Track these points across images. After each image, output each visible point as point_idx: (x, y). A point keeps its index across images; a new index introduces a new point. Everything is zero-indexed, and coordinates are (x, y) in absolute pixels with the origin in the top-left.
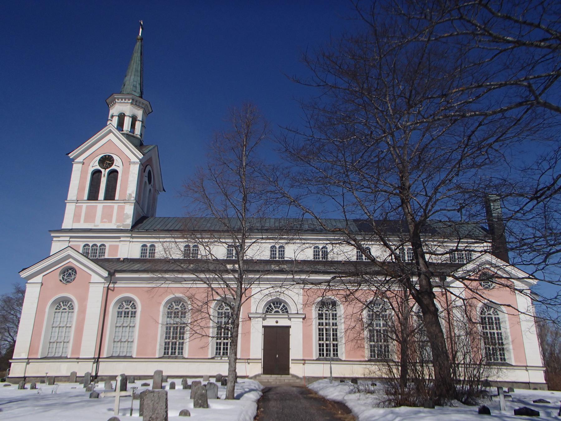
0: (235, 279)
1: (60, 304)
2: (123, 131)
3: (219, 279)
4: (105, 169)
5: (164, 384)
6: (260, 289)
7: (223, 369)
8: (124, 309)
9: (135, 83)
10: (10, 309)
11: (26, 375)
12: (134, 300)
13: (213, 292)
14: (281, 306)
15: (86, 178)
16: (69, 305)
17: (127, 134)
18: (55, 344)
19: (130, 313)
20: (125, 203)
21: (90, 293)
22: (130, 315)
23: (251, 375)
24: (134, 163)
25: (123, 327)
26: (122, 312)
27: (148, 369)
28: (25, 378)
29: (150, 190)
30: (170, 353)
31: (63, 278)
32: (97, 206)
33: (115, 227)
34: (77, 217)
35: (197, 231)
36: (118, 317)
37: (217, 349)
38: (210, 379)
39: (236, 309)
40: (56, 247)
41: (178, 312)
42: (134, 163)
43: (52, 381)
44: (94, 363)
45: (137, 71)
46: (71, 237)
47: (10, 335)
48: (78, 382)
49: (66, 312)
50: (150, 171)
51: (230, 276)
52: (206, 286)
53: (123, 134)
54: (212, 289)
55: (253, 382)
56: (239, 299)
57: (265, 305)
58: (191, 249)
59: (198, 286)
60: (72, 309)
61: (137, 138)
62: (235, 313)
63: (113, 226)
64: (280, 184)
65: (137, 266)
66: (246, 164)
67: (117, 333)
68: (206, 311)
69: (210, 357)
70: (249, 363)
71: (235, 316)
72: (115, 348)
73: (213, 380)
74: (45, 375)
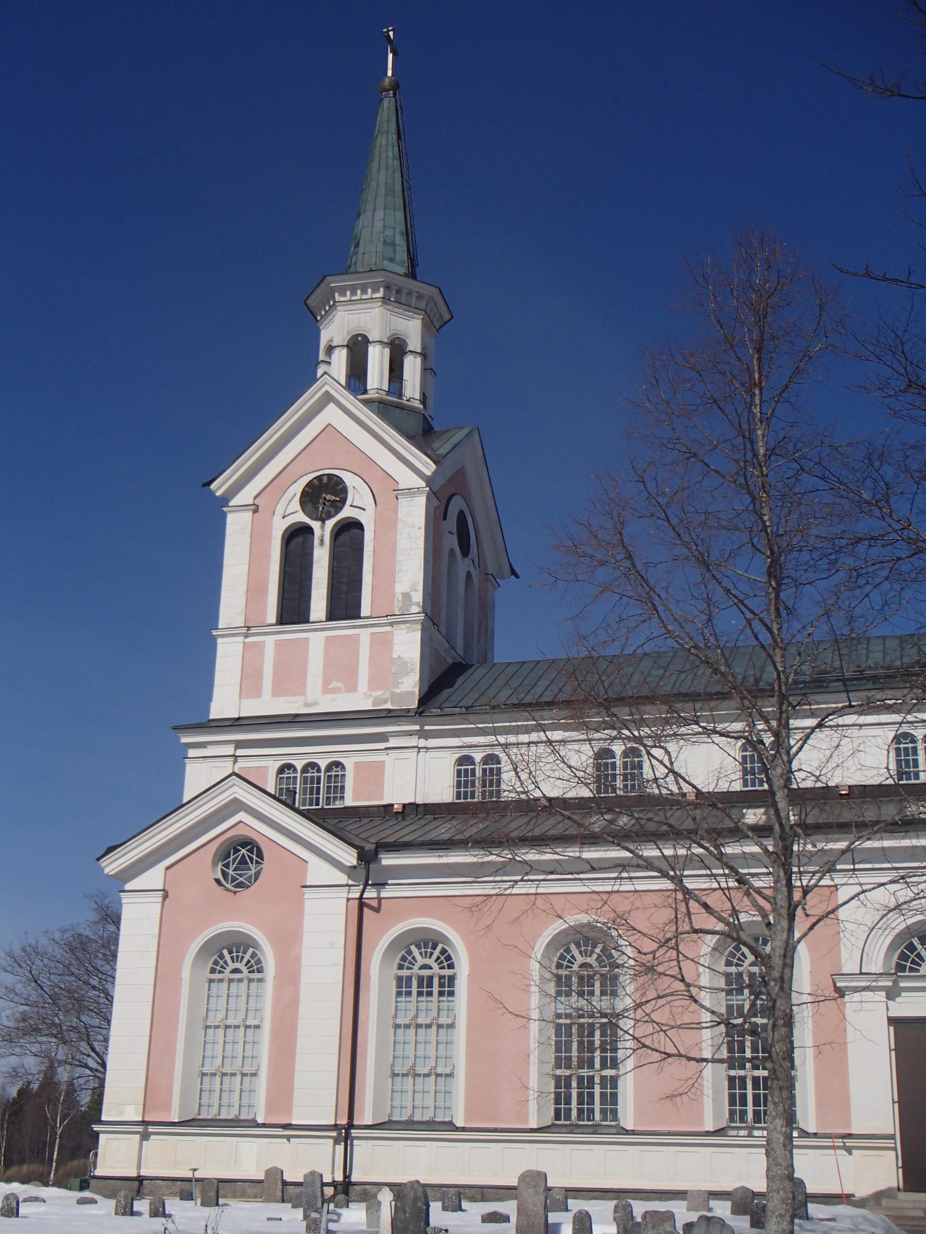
0: (765, 859)
1: (222, 956)
2: (365, 392)
3: (710, 860)
4: (323, 521)
5: (553, 1217)
6: (858, 889)
7: (746, 1168)
9: (389, 233)
10: (88, 973)
11: (144, 1172)
12: (446, 940)
13: (692, 903)
14: (437, 953)
15: (268, 556)
16: (247, 957)
17: (381, 402)
18: (218, 1079)
19: (436, 981)
20: (391, 624)
21: (306, 919)
22: (436, 989)
23: (862, 1191)
24: (411, 492)
25: (418, 1026)
26: (409, 978)
27: (499, 1164)
28: (140, 1179)
29: (469, 575)
30: (574, 1113)
31: (225, 874)
32: (307, 639)
33: (367, 705)
34: (250, 683)
35: (621, 700)
36: (399, 994)
37: (732, 1102)
38: (712, 1203)
39: (777, 961)
40: (198, 775)
41: (591, 977)
42: (411, 492)
43: (212, 1194)
44: (336, 1142)
45: (390, 192)
46: (239, 744)
47: (93, 1049)
48: (289, 1201)
49: (221, 981)
50: (461, 514)
51: (747, 849)
52: (666, 884)
53: (366, 402)
54: (687, 892)
55: (865, 1218)
56: (785, 924)
57: (892, 946)
58: (619, 762)
59: (641, 886)
60: (260, 971)
61: (413, 410)
62: (776, 974)
63: (360, 701)
64: (901, 507)
65: (443, 830)
66: (771, 452)
67: (400, 1047)
68: (675, 971)
69: (709, 1125)
70: (849, 1150)
71: (774, 987)
72: (397, 1096)
73: (722, 1209)
74: (189, 1175)
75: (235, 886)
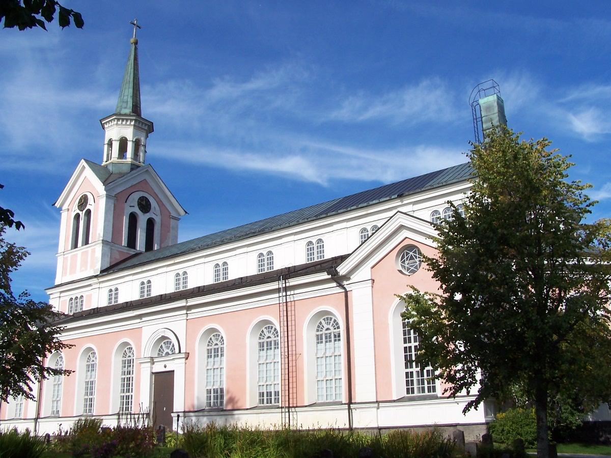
8: (324, 331)
15: (70, 226)
22: (324, 340)
26: (321, 335)
36: (318, 343)
46: (61, 292)
75: (409, 273)
